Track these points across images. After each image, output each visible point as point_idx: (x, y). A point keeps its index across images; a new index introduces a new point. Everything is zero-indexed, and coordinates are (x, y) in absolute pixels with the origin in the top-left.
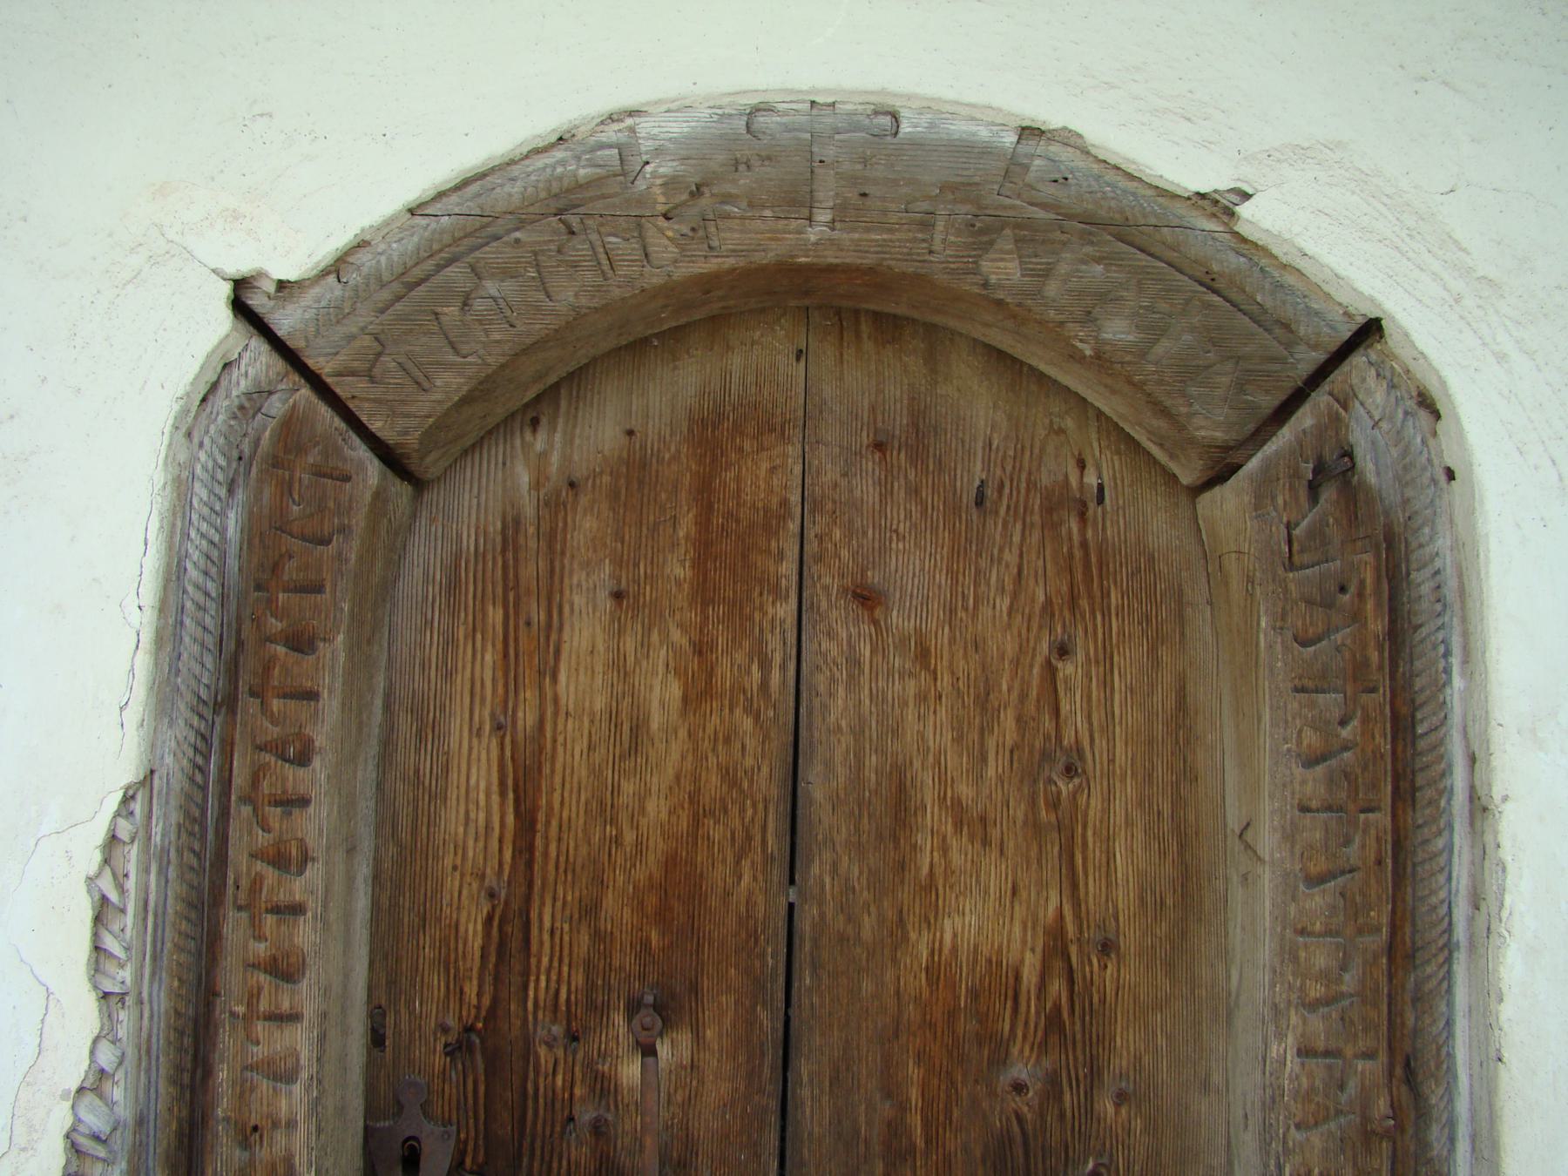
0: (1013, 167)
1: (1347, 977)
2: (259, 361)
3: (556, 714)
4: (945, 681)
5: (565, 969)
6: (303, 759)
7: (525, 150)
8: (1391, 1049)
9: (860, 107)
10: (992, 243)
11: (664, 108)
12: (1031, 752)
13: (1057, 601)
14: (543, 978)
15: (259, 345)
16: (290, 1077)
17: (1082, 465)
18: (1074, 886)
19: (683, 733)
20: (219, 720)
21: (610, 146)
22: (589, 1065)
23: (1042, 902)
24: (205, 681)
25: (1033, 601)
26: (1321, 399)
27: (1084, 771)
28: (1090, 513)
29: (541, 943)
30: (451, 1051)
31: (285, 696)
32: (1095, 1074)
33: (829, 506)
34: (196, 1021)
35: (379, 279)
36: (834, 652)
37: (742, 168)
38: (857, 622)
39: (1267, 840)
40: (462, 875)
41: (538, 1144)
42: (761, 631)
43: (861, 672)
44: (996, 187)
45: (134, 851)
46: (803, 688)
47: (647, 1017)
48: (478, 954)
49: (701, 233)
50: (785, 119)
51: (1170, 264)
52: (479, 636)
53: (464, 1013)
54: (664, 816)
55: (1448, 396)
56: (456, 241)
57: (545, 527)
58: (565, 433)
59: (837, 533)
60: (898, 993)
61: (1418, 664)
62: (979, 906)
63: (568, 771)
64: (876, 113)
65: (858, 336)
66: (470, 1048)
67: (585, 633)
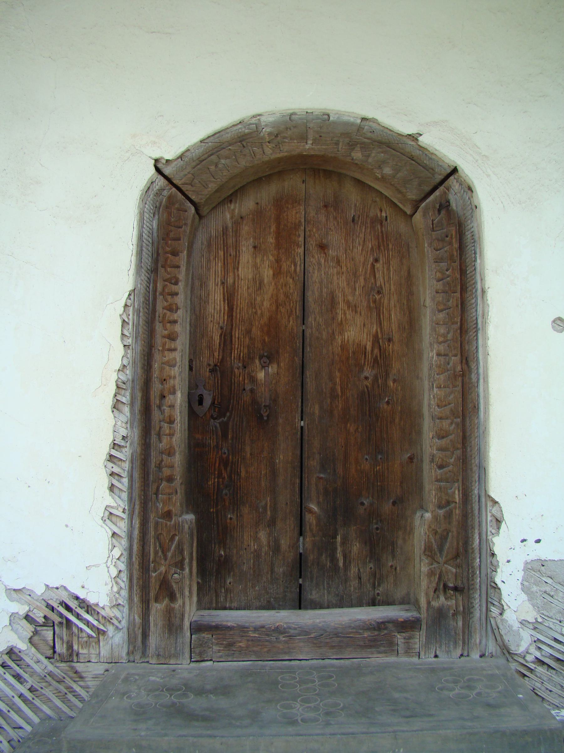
0: (360, 128)
1: (449, 335)
2: (161, 182)
3: (238, 279)
4: (344, 269)
5: (242, 348)
6: (176, 283)
7: (231, 125)
8: (461, 355)
9: (320, 113)
10: (354, 148)
11: (268, 114)
12: (368, 288)
13: (374, 247)
14: (236, 351)
15: (160, 177)
16: (174, 366)
17: (381, 211)
18: (380, 324)
19: (273, 284)
20: (152, 275)
21: (253, 124)
22: (249, 374)
23: (372, 328)
24: (149, 264)
25: (368, 247)
26: (442, 188)
27: (383, 293)
28: (384, 223)
29: (235, 341)
30: (211, 371)
31: (171, 267)
32: (387, 375)
33: (312, 222)
34: (148, 353)
35: (193, 159)
36: (314, 261)
37: (288, 129)
38: (320, 253)
39: (428, 302)
40: (213, 323)
41: (235, 396)
42: (294, 256)
43: (321, 266)
44: (355, 134)
45: (131, 308)
46: (306, 271)
47: (265, 359)
48: (218, 344)
49: (278, 147)
50: (300, 117)
51: (401, 153)
52: (217, 259)
53: (215, 361)
54: (268, 306)
55: (474, 186)
56: (213, 149)
57: (234, 229)
58: (239, 204)
59: (314, 230)
60: (333, 353)
61: (467, 256)
62: (355, 329)
63: (242, 295)
64: (324, 115)
65: (319, 177)
66: (216, 371)
67: (246, 257)
